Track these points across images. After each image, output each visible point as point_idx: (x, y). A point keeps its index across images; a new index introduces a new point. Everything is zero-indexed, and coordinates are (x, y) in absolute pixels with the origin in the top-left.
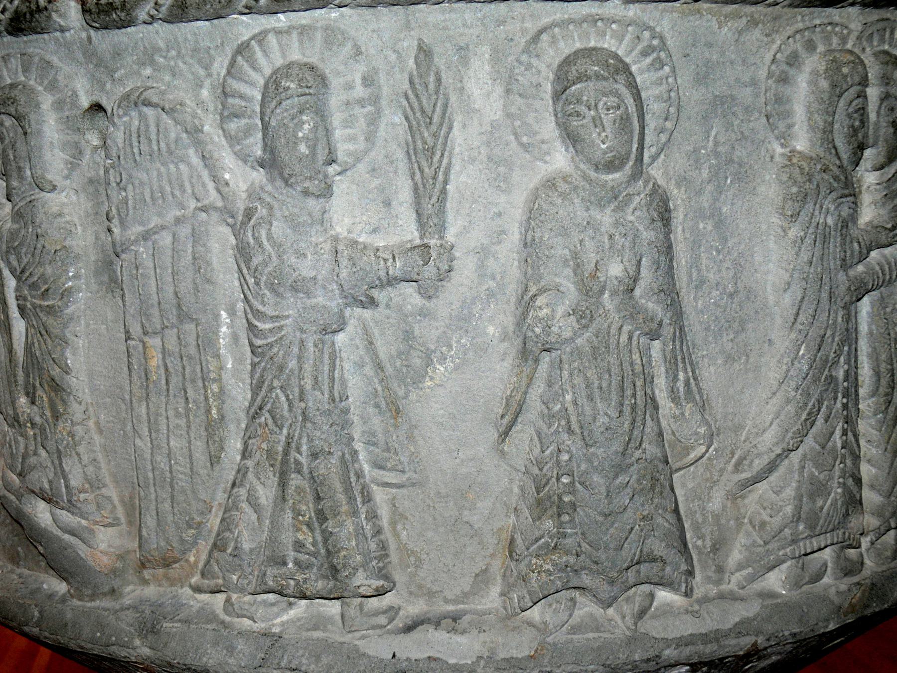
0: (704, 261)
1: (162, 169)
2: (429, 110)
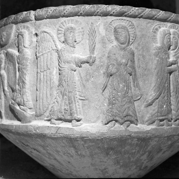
0: (140, 63)
1: (46, 43)
2: (92, 33)
